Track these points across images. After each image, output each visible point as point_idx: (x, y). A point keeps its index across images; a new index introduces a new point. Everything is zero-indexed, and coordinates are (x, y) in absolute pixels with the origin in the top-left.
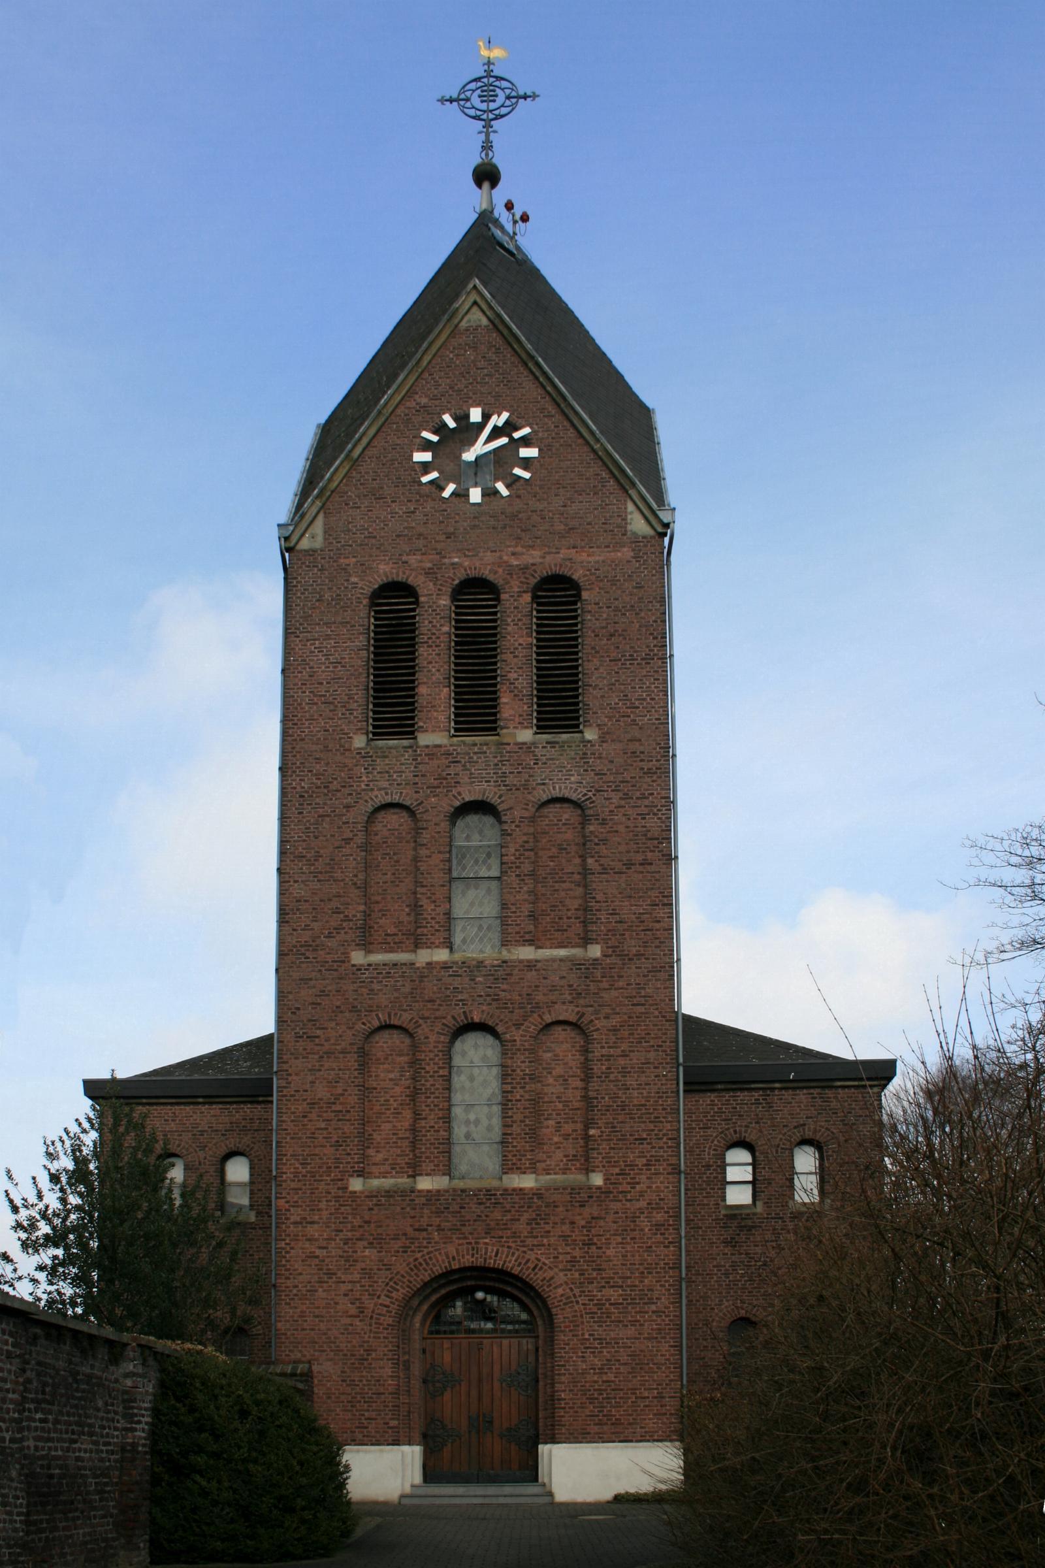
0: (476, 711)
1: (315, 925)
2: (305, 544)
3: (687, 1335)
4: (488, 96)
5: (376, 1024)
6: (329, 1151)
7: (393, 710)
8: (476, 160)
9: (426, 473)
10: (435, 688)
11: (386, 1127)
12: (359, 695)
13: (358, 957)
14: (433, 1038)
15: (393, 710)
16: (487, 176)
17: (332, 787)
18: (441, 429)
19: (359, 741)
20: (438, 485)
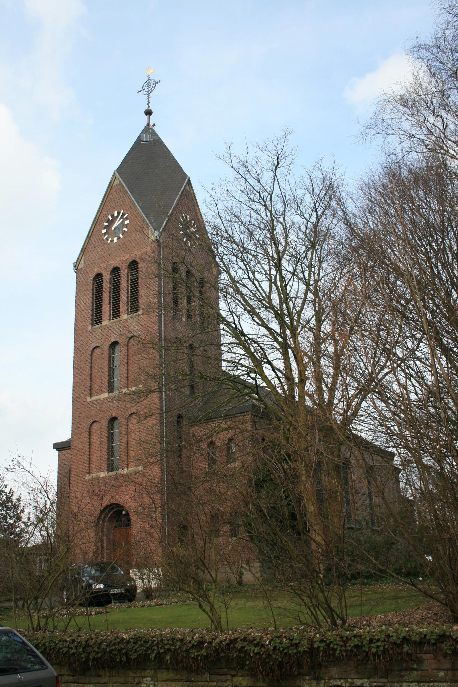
0: (116, 313)
1: (80, 390)
2: (79, 267)
3: (47, 659)
4: (149, 86)
5: (92, 421)
6: (81, 466)
7: (97, 319)
8: (146, 108)
9: (108, 240)
10: (106, 308)
11: (95, 455)
12: (90, 312)
13: (89, 399)
14: (104, 424)
15: (97, 319)
16: (149, 113)
17: (84, 344)
18: (105, 234)
19: (90, 327)
20: (112, 241)
